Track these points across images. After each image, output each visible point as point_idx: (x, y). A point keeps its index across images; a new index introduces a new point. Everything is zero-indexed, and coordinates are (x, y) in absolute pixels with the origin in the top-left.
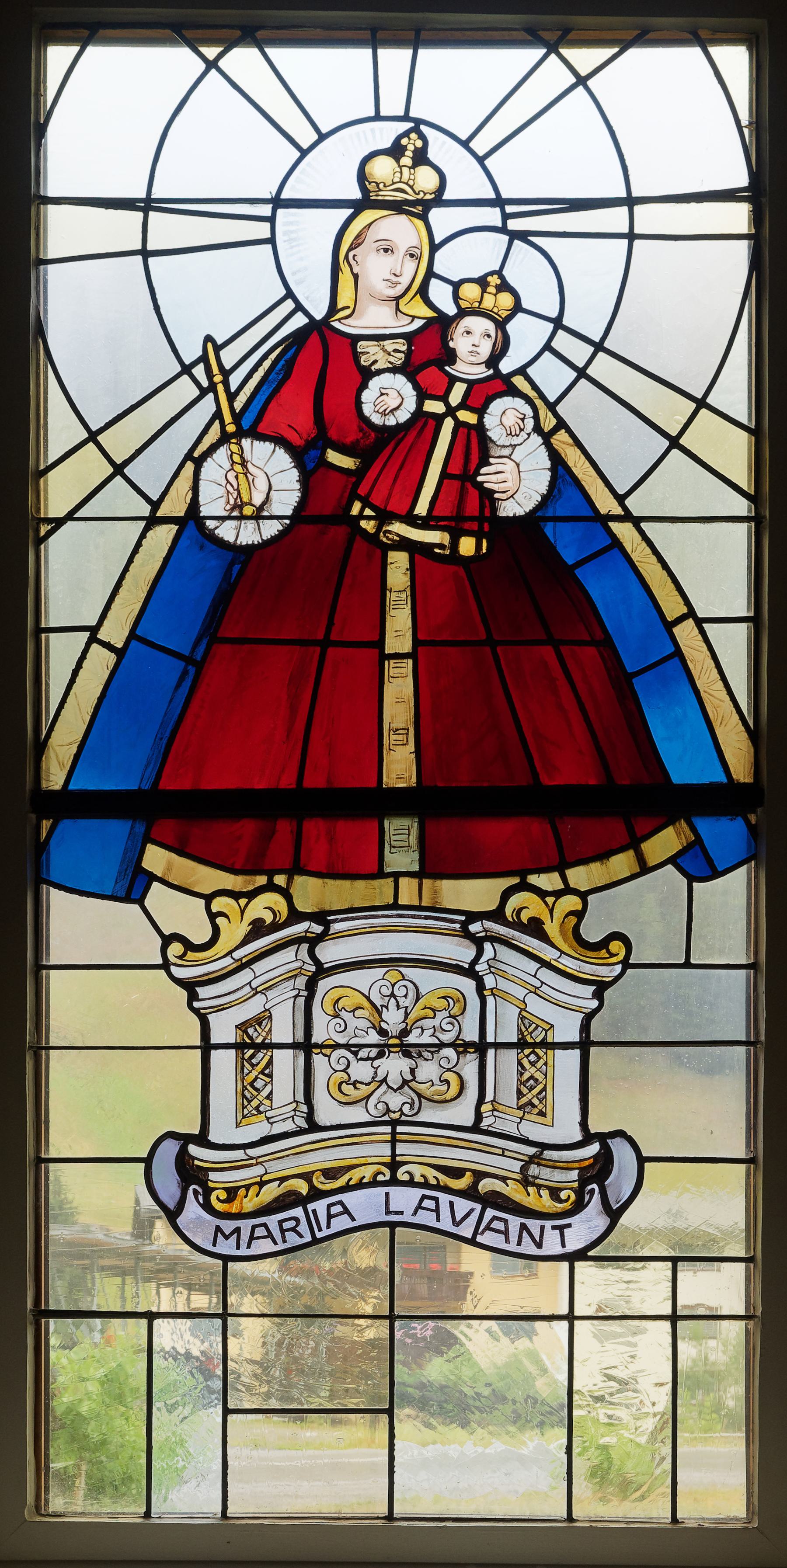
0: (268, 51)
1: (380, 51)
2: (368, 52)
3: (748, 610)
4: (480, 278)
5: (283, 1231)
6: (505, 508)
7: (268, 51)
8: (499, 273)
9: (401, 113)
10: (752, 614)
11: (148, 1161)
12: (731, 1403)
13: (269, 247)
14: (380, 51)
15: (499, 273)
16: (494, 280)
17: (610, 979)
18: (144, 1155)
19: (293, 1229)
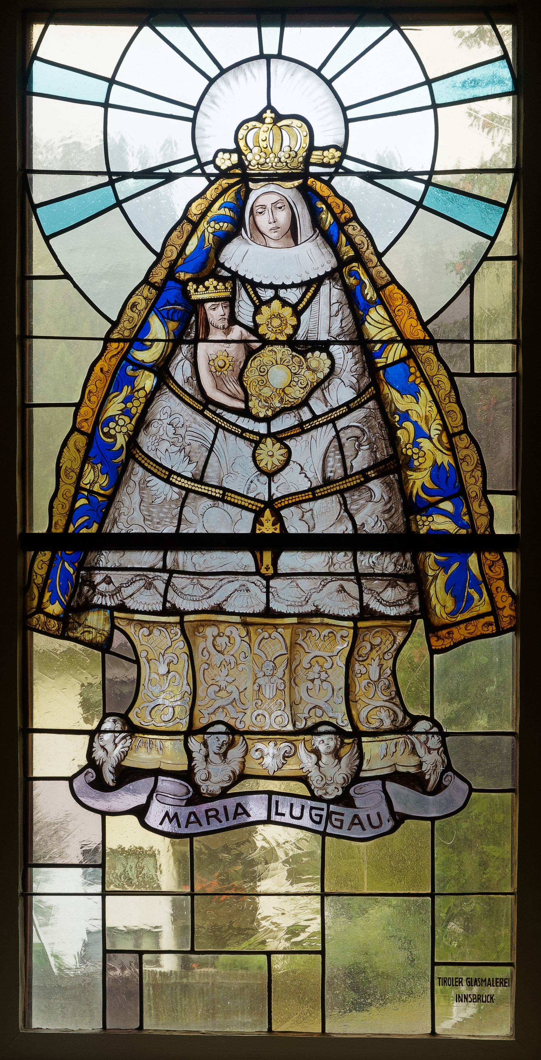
0: (196, 29)
1: (264, 29)
2: (255, 30)
3: (513, 335)
4: (257, 116)
5: (208, 817)
6: (160, 866)
7: (196, 29)
8: (269, 107)
9: (346, 104)
10: (515, 338)
11: (104, 814)
12: (505, 751)
13: (190, 124)
14: (264, 29)
15: (269, 107)
16: (269, 115)
17: (444, 777)
18: (99, 817)
19: (215, 816)
